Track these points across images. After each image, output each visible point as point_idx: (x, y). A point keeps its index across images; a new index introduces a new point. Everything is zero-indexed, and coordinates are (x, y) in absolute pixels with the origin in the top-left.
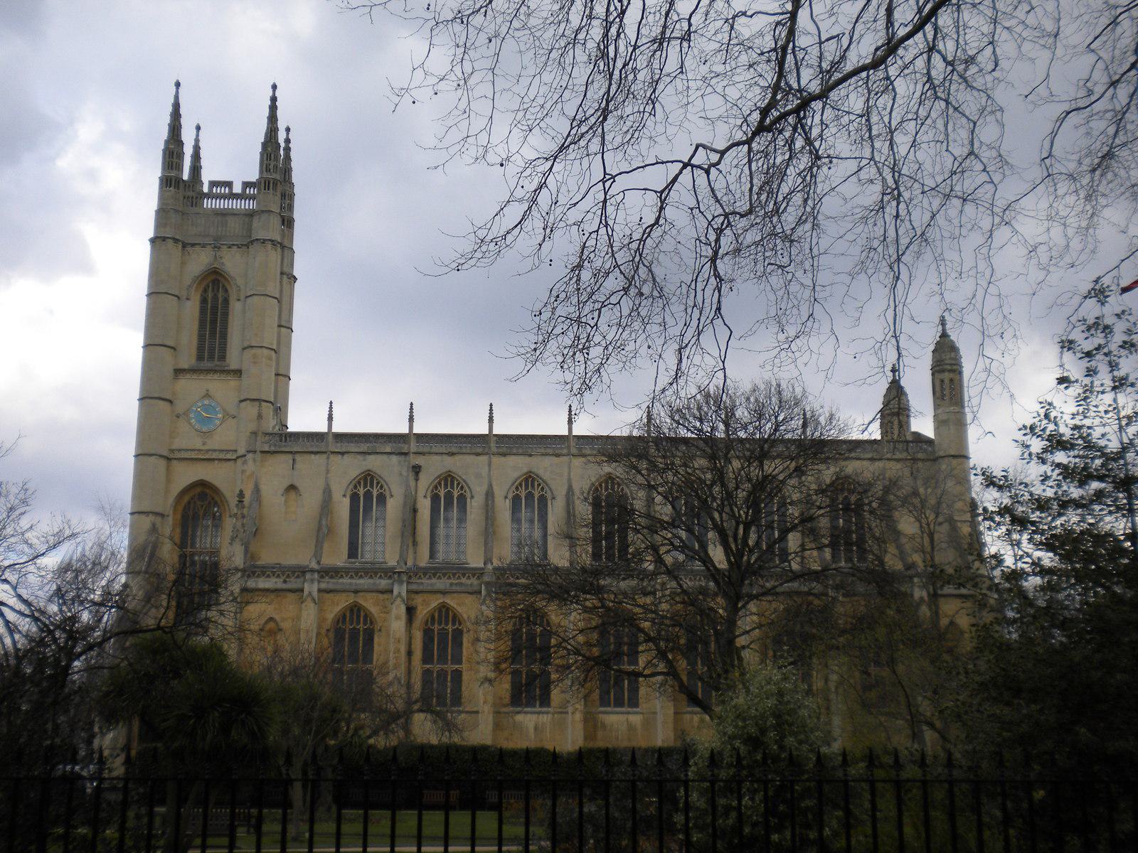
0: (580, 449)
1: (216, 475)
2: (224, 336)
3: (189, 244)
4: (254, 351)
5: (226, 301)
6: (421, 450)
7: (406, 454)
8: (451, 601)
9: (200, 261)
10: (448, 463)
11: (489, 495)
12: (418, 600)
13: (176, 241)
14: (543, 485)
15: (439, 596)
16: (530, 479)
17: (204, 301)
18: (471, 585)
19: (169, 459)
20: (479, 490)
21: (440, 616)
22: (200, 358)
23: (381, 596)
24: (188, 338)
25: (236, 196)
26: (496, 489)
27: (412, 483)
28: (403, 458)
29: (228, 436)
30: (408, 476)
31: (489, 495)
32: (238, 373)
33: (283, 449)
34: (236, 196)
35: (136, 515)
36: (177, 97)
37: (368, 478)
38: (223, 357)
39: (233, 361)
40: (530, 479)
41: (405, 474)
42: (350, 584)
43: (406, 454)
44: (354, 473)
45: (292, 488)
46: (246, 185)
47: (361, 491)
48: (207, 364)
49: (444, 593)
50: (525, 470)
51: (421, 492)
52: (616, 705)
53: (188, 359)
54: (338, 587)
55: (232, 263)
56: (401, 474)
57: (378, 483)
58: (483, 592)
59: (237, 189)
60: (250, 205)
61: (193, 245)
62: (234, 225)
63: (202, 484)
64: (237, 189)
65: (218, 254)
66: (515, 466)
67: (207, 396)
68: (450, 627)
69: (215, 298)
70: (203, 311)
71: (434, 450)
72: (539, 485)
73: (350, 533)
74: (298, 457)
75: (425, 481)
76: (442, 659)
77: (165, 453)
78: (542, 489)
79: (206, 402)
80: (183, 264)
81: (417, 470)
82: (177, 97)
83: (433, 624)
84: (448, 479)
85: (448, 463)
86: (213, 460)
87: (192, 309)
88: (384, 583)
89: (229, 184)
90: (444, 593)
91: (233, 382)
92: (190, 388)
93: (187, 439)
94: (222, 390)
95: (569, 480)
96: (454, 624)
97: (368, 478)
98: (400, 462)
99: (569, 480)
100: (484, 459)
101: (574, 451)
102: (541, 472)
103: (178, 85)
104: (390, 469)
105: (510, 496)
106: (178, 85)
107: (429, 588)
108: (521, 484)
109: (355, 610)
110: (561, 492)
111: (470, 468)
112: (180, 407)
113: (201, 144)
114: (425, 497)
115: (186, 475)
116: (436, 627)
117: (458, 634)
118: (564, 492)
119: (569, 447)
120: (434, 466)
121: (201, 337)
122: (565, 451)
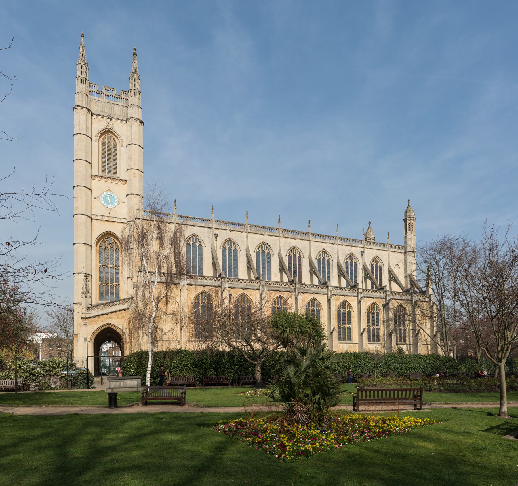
0: (283, 235)
3: (95, 114)
6: (217, 227)
7: (211, 228)
8: (246, 292)
13: (89, 111)
15: (242, 290)
18: (255, 286)
21: (343, 305)
22: (103, 171)
27: (215, 242)
28: (209, 230)
30: (212, 238)
31: (247, 250)
33: (257, 232)
38: (115, 173)
41: (211, 237)
42: (201, 282)
43: (211, 228)
44: (348, 252)
50: (262, 241)
51: (218, 247)
52: (377, 341)
53: (97, 170)
56: (209, 237)
57: (198, 240)
65: (110, 122)
67: (109, 190)
68: (347, 310)
71: (223, 228)
72: (267, 248)
73: (330, 271)
78: (269, 249)
79: (109, 193)
81: (216, 236)
83: (340, 308)
84: (229, 241)
90: (314, 293)
95: (280, 247)
96: (317, 307)
98: (208, 232)
99: (280, 247)
101: (281, 235)
105: (256, 251)
107: (237, 286)
108: (260, 247)
114: (184, 244)
116: (342, 310)
118: (278, 252)
119: (279, 233)
122: (277, 235)
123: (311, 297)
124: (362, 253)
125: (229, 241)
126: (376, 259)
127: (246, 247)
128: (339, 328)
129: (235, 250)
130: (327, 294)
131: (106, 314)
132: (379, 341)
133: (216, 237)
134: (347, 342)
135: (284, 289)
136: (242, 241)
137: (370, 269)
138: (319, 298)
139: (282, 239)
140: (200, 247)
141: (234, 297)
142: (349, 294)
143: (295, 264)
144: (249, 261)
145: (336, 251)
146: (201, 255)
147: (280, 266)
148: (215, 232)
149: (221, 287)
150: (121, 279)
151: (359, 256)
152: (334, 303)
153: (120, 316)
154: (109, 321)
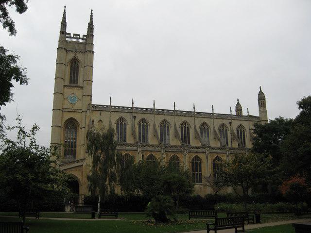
1: (77, 116)
2: (77, 77)
4: (88, 81)
5: (78, 67)
9: (71, 56)
10: (143, 116)
11: (154, 125)
12: (144, 153)
13: (65, 49)
14: (168, 124)
16: (165, 121)
17: (71, 67)
19: (62, 111)
20: (151, 124)
22: (70, 83)
23: (134, 152)
24: (67, 77)
25: (81, 39)
26: (156, 123)
27: (134, 121)
29: (78, 105)
31: (154, 125)
32: (82, 87)
34: (81, 39)
35: (54, 127)
36: (65, 10)
37: (121, 119)
38: (77, 83)
39: (80, 83)
40: (165, 121)
45: (100, 120)
46: (84, 36)
47: (120, 122)
48: (72, 85)
49: (151, 151)
51: (136, 124)
53: (67, 83)
54: (122, 149)
55: (80, 57)
58: (162, 151)
59: (81, 37)
60: (84, 41)
61: (69, 51)
62: (81, 47)
63: (69, 119)
64: (81, 37)
66: (160, 118)
69: (75, 66)
70: (71, 70)
74: (102, 113)
75: (137, 120)
76: (197, 171)
77: (61, 109)
80: (66, 56)
81: (135, 117)
82: (65, 10)
84: (143, 120)
85: (143, 116)
86: (75, 112)
87: (68, 69)
88: (135, 148)
89: (79, 35)
90: (197, 152)
91: (81, 90)
92: (68, 91)
93: (67, 106)
94: (78, 92)
97: (121, 119)
100: (153, 115)
102: (168, 120)
103: (65, 7)
104: (128, 117)
106: (65, 7)
109: (197, 157)
110: (173, 125)
111: (149, 118)
112: (66, 96)
113: (94, 24)
115: (67, 116)
116: (216, 162)
117: (200, 163)
120: (139, 117)
121: (71, 77)
123: (195, 155)
124: (230, 123)
125: (143, 120)
126: (240, 126)
127: (153, 123)
128: (193, 174)
129: (208, 129)
130: (205, 153)
131: (70, 169)
132: (201, 183)
133: (135, 118)
134: (199, 184)
135: (177, 151)
136: (151, 120)
137: (236, 133)
138: (200, 155)
139: (176, 117)
140: (188, 128)
141: (145, 157)
142: (221, 152)
143: (185, 135)
144: (156, 131)
145: (212, 122)
146: (125, 129)
147: (196, 134)
148: (134, 115)
149: (137, 150)
150: (77, 146)
151: (228, 125)
152: (210, 158)
153: (78, 170)
154: (71, 173)
